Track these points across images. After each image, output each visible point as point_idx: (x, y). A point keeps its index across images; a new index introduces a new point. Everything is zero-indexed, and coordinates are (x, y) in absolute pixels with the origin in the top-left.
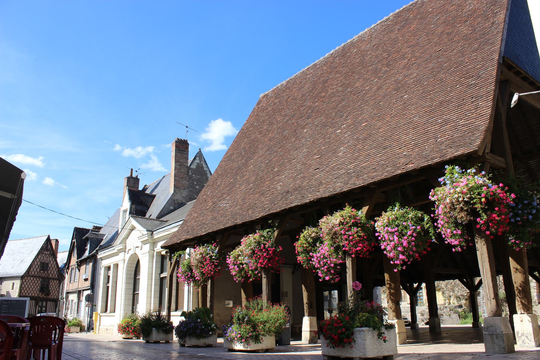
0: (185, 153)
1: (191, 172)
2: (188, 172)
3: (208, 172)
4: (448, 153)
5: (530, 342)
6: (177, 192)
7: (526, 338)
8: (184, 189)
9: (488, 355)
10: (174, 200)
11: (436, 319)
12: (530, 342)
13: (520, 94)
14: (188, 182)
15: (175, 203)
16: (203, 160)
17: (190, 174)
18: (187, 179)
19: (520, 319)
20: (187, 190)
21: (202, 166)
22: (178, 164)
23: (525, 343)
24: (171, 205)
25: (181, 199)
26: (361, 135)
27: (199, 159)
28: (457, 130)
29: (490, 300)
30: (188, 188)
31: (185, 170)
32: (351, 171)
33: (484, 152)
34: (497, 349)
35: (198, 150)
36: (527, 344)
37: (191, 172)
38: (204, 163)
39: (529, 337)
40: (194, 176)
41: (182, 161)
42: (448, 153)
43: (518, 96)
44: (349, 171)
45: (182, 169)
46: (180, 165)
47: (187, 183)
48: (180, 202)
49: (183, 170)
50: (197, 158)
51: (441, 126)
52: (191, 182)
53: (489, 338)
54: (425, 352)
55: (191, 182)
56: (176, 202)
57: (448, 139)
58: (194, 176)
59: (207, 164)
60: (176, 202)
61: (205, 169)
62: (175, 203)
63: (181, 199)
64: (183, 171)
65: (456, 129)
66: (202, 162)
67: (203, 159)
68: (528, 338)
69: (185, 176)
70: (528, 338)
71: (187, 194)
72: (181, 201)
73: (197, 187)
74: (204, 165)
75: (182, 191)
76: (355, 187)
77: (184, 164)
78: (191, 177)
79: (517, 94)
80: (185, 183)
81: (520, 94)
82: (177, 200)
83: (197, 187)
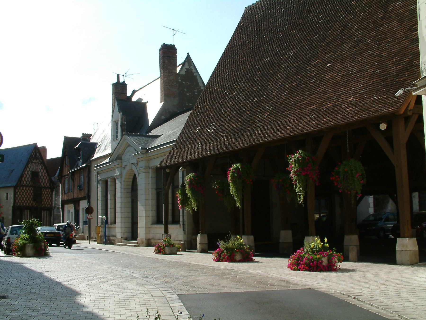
17: (180, 81)
27: (188, 65)
37: (181, 79)
40: (184, 82)
50: (186, 63)
58: (184, 82)
66: (191, 67)
83: (188, 94)
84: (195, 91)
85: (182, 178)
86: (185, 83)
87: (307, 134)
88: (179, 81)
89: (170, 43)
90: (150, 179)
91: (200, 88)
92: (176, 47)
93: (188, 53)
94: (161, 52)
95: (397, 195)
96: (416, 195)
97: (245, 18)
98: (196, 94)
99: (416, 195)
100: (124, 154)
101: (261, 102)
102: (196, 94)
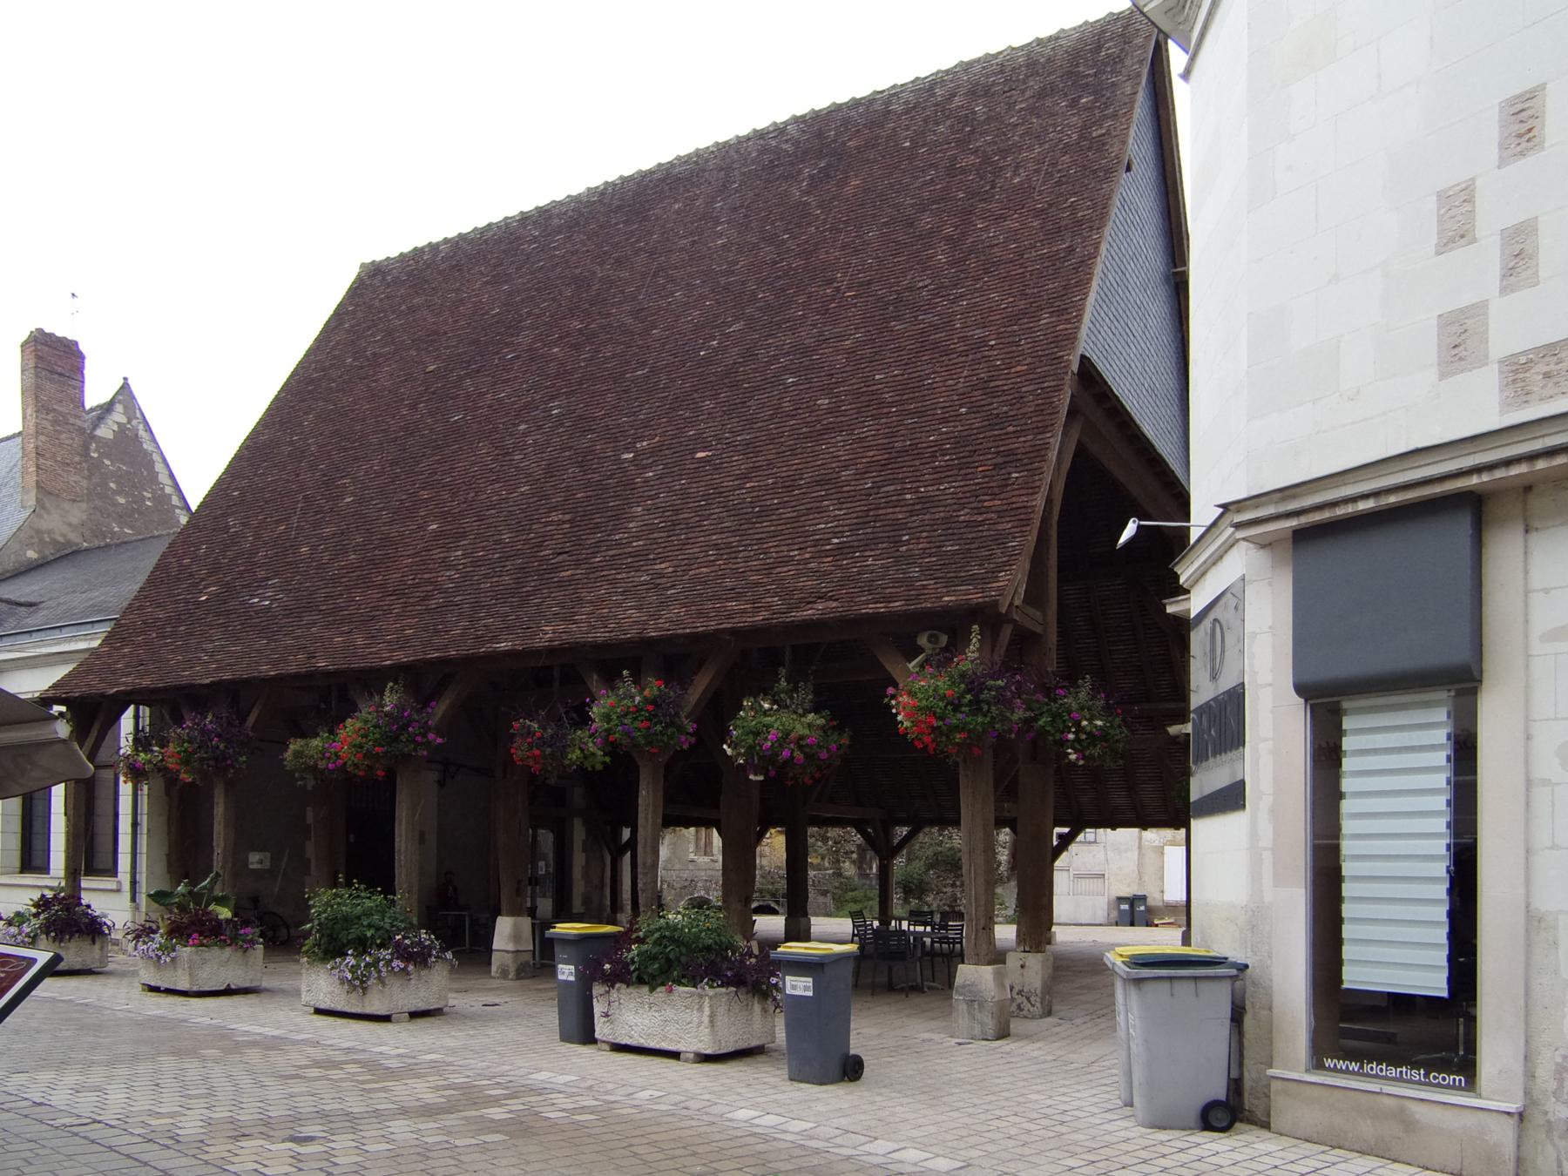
0: (74, 382)
1: (97, 450)
2: (86, 449)
3: (156, 457)
4: (926, 592)
5: (1032, 1009)
6: (48, 505)
7: (1025, 1001)
8: (74, 501)
9: (960, 1044)
10: (39, 532)
11: (803, 920)
12: (1032, 1009)
13: (1142, 523)
14: (89, 478)
15: (42, 541)
16: (138, 415)
17: (95, 455)
18: (81, 469)
19: (1021, 962)
20: (84, 506)
21: (137, 435)
22: (50, 417)
23: (1022, 1010)
24: (30, 546)
25: (65, 529)
26: (694, 485)
27: (125, 413)
28: (950, 531)
29: (977, 930)
30: (89, 500)
31: (73, 439)
32: (664, 580)
33: (1011, 604)
34: (977, 1031)
35: (122, 381)
36: (1025, 1013)
37: (97, 450)
38: (141, 427)
39: (1032, 999)
40: (107, 462)
41: (60, 409)
42: (926, 592)
43: (1135, 526)
44: (658, 581)
45: (64, 436)
46: (55, 422)
47: (84, 483)
48: (62, 540)
49: (67, 438)
50: (119, 408)
51: (912, 513)
52: (96, 479)
53: (965, 1007)
54: (624, 873)
55: (96, 479)
56: (48, 540)
57: (927, 551)
58: (107, 462)
59: (151, 432)
60: (48, 540)
61: (148, 446)
62: (42, 541)
63: (65, 529)
64: (67, 442)
65: (949, 529)
66: (134, 422)
67: (138, 411)
68: (1030, 1002)
69: (77, 459)
70: (1030, 1002)
71: (84, 517)
72: (64, 536)
73: (122, 501)
74: (142, 433)
75: (66, 505)
76: (680, 631)
77: (72, 420)
78: (96, 466)
79: (1134, 522)
80: (75, 482)
81: (1142, 523)
82: (49, 532)
83: (122, 501)
84: (145, 494)
85: (121, 830)
86: (113, 464)
87: (650, 642)
88: (92, 454)
89: (60, 328)
90: (109, 981)
91: (163, 489)
92: (82, 347)
93: (125, 379)
94: (28, 351)
95: (906, 840)
96: (1005, 836)
97: (357, 291)
98: (148, 503)
99: (1005, 836)
100: (1396, 1166)
101: (821, 442)
102: (148, 503)
